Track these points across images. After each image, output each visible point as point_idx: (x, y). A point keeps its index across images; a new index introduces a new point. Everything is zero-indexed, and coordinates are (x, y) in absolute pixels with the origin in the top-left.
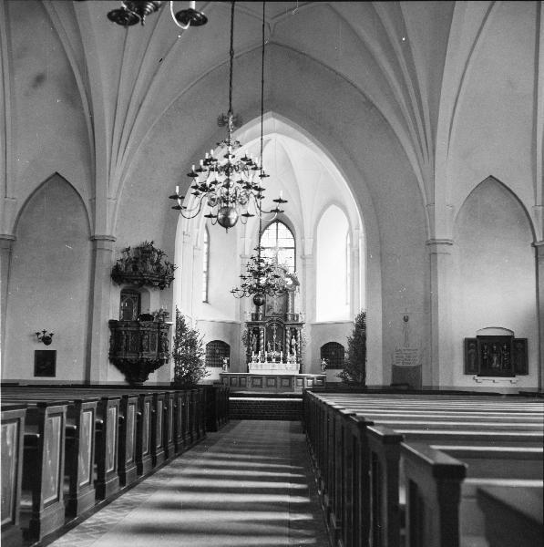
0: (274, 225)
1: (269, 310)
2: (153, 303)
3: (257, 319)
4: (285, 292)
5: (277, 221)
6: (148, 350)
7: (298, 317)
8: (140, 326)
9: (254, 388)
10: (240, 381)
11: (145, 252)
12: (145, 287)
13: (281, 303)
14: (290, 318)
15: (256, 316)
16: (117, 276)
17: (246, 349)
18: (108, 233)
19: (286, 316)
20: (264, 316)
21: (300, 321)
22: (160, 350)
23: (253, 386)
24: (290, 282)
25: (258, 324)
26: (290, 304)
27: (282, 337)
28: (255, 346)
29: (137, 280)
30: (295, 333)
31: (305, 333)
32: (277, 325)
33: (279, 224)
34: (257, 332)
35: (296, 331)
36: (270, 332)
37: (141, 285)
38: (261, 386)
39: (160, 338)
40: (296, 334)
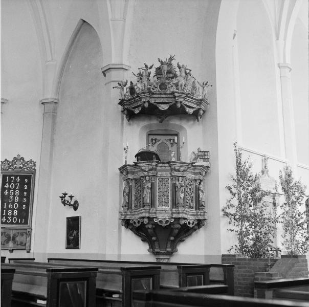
2: (192, 138)
6: (152, 204)
11: (166, 72)
16: (136, 108)
18: (114, 61)
22: (175, 204)
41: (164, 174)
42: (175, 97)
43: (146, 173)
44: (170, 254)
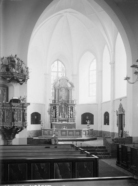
0: (56, 63)
1: (60, 98)
3: (55, 102)
4: (68, 90)
5: (58, 60)
7: (73, 101)
8: (11, 106)
9: (69, 137)
10: (49, 132)
12: (11, 83)
13: (66, 95)
14: (70, 102)
15: (55, 101)
17: (50, 116)
19: (68, 101)
20: (58, 101)
21: (74, 103)
23: (62, 135)
24: (69, 86)
25: (56, 105)
26: (70, 94)
27: (67, 111)
28: (54, 115)
29: (9, 77)
30: (72, 108)
31: (75, 108)
32: (64, 105)
33: (59, 61)
34: (55, 108)
35: (72, 108)
36: (61, 108)
37: (10, 81)
38: (66, 135)
39: (23, 113)
40: (72, 109)
41: (20, 108)
42: (13, 75)
43: (15, 108)
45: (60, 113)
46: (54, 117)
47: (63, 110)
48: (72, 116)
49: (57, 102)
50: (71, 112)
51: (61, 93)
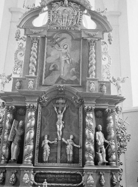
1: (49, 73)
44: (132, 106)
45: (47, 141)
46: (14, 157)
47: (60, 127)
48: (102, 158)
49: (31, 84)
50: (100, 134)
51: (52, 54)
